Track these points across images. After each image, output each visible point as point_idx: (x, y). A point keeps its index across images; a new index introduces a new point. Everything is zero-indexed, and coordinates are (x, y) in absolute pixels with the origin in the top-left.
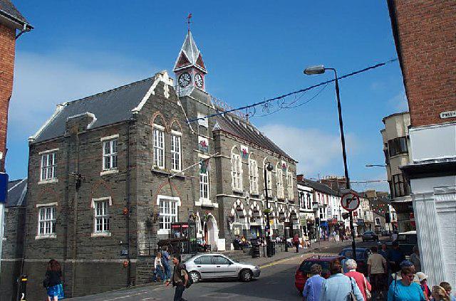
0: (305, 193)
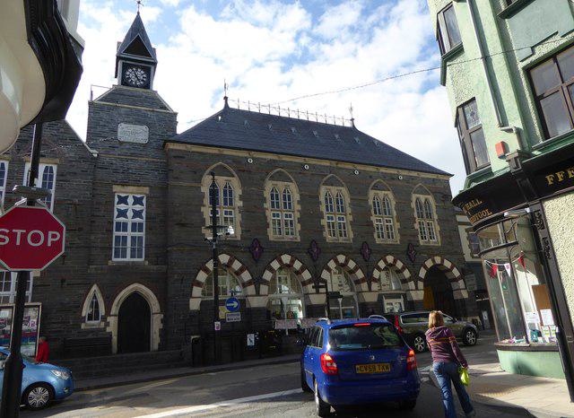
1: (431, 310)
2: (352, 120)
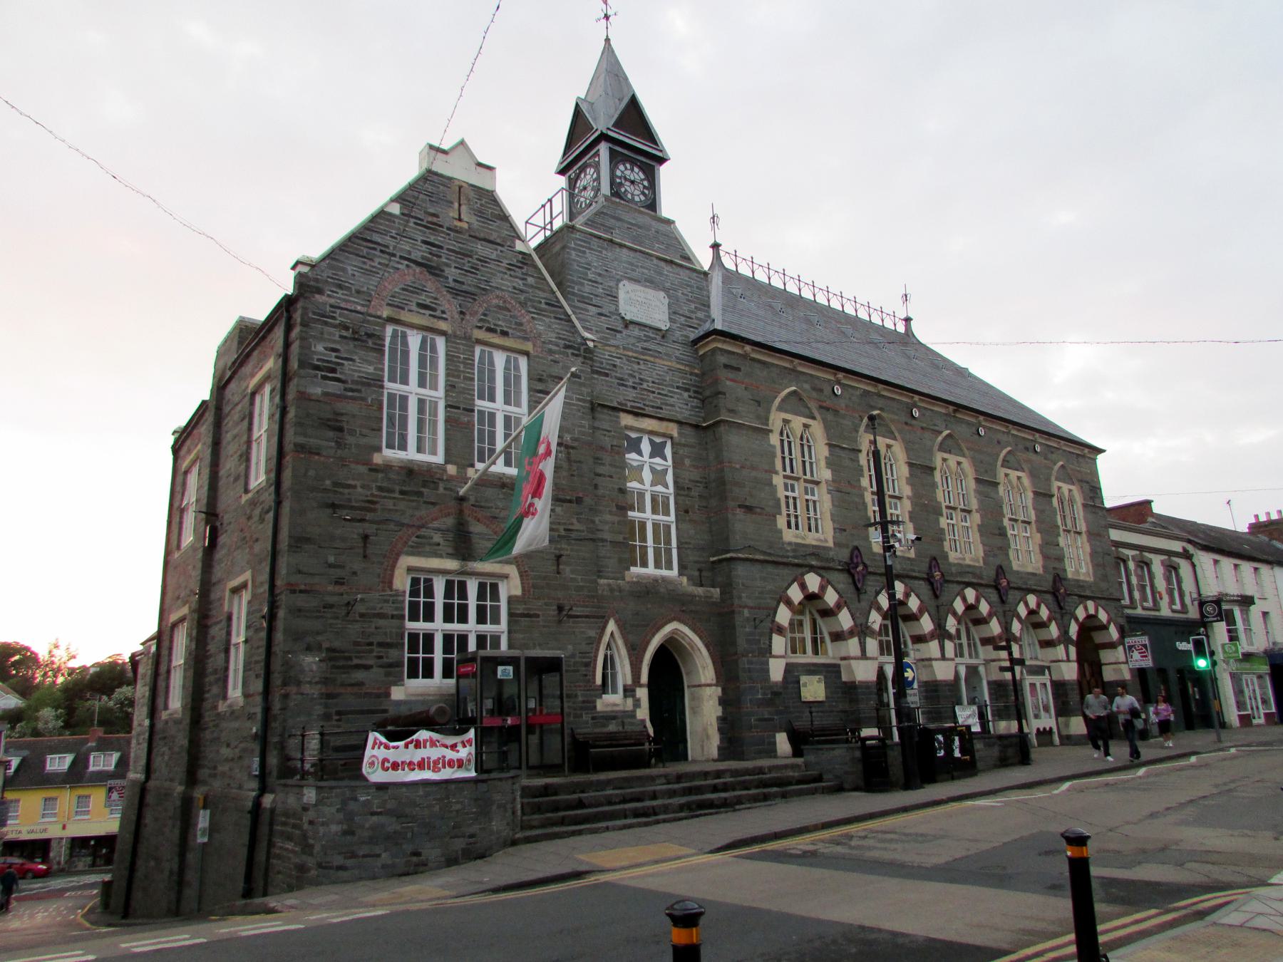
0: (1130, 553)
1: (403, 627)
2: (908, 320)
